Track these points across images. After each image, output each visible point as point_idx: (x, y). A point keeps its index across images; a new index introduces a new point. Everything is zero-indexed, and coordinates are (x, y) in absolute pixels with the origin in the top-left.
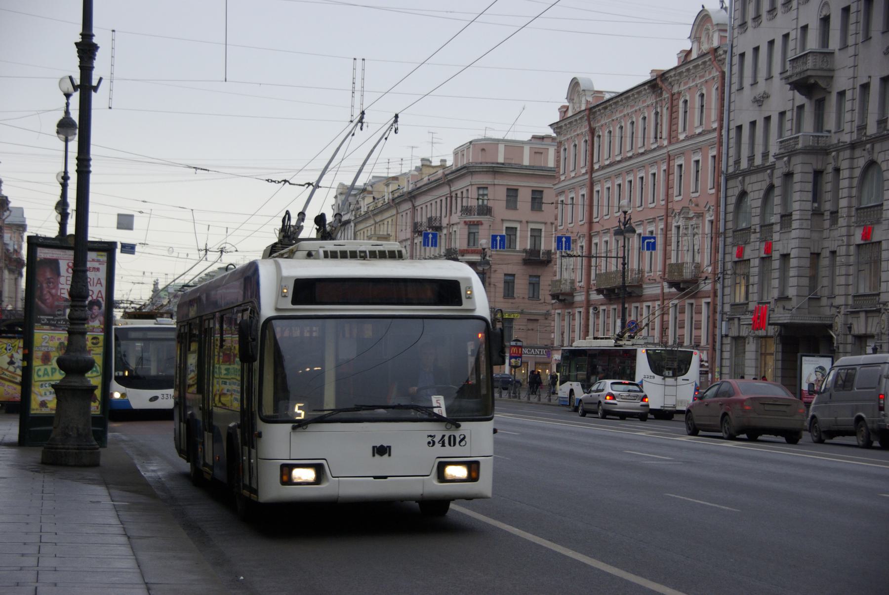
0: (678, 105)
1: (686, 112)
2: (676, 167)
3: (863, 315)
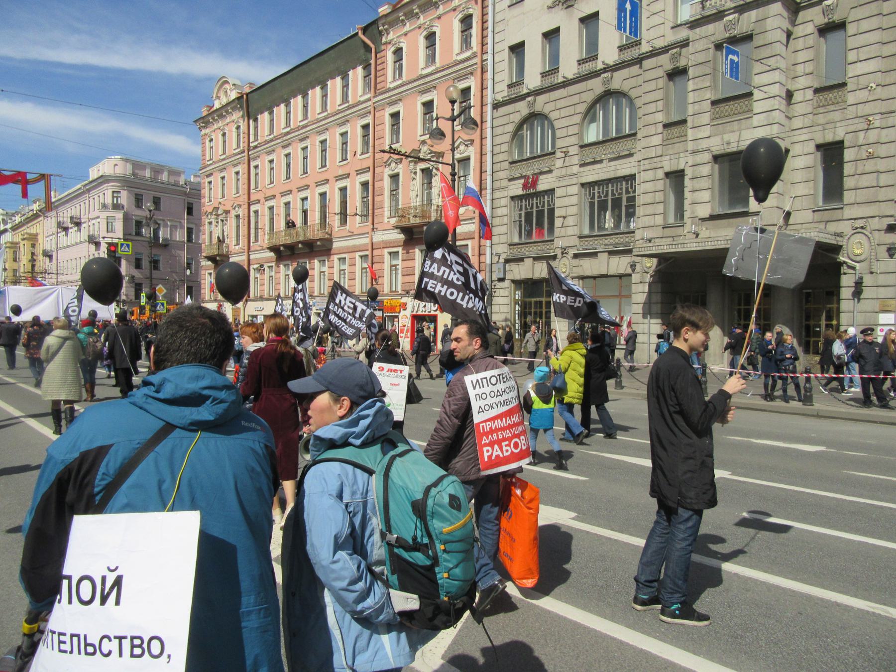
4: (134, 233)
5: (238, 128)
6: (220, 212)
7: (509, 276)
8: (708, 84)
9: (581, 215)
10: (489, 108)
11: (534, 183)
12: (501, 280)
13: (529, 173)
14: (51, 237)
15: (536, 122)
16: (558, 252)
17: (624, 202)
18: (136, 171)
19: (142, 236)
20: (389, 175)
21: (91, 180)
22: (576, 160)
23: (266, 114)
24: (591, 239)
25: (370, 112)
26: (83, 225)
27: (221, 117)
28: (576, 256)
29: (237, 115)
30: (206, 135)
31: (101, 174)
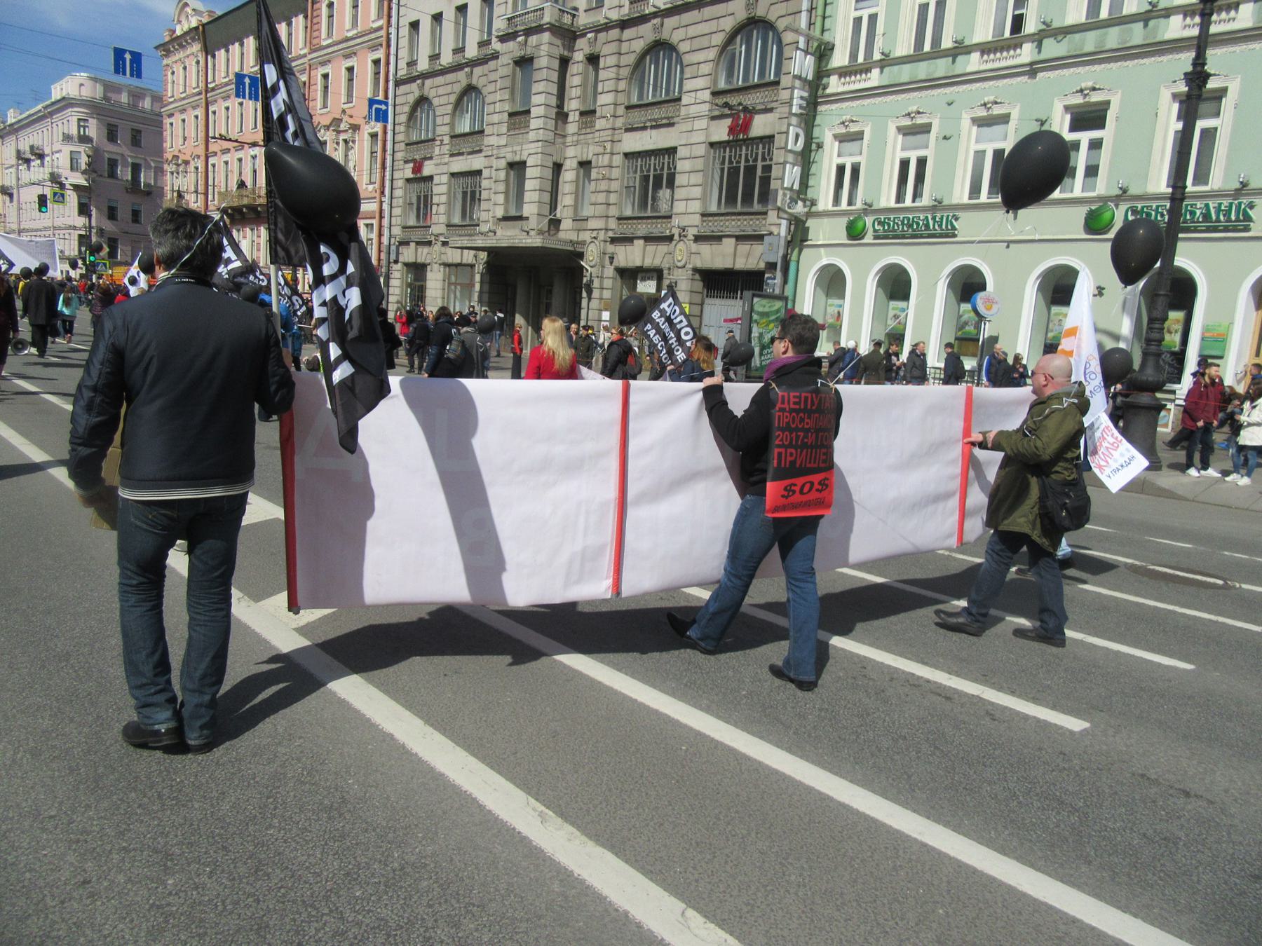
0: (320, 9)
1: (331, 16)
2: (319, 77)
3: (413, 245)
4: (106, 174)
5: (198, 62)
6: (343, 126)
7: (401, 259)
8: (507, 97)
9: (449, 205)
10: (391, 84)
11: (746, 126)
12: (396, 262)
13: (417, 157)
14: (11, 170)
15: (755, 32)
16: (676, 232)
17: (759, 172)
18: (109, 95)
19: (117, 178)
20: (369, 134)
21: (53, 100)
22: (446, 149)
23: (223, 51)
24: (710, 218)
25: (381, 45)
26: (47, 159)
27: (182, 47)
28: (698, 239)
29: (196, 47)
30: (167, 65)
31: (64, 94)
